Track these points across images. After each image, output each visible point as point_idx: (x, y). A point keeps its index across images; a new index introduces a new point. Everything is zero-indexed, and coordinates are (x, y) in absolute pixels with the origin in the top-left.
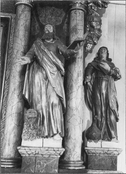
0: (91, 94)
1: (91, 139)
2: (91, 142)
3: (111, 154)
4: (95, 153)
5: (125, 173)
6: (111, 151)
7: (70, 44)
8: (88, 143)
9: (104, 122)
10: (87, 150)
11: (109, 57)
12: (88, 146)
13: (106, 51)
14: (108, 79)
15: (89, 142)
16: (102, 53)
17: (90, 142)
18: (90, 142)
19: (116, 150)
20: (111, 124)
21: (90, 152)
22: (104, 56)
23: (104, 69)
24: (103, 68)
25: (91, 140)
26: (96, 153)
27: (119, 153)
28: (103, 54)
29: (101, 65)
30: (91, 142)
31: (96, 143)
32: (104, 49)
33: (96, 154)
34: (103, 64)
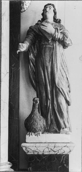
0: (34, 71)
1: (30, 132)
2: (31, 136)
3: (59, 151)
4: (37, 151)
5: (2, 1)
6: (58, 147)
7: (22, 66)
8: (27, 136)
9: (50, 105)
10: (24, 147)
11: (58, 17)
12: (26, 142)
13: (52, 9)
14: (53, 47)
15: (28, 135)
16: (46, 12)
17: (29, 136)
18: (29, 136)
19: (65, 145)
20: (59, 109)
21: (29, 150)
22: (50, 16)
23: (46, 32)
24: (45, 31)
25: (31, 133)
26: (38, 151)
27: (71, 149)
28: (48, 13)
29: (42, 27)
30: (31, 136)
31: (38, 136)
32: (50, 6)
33: (39, 152)
34: (46, 25)
